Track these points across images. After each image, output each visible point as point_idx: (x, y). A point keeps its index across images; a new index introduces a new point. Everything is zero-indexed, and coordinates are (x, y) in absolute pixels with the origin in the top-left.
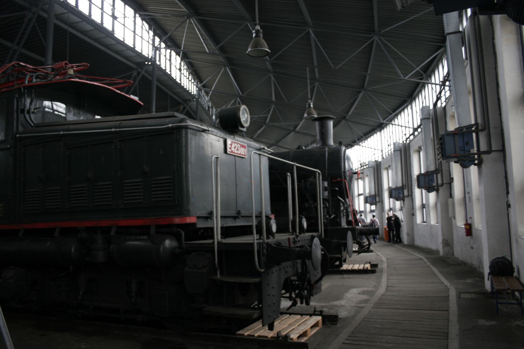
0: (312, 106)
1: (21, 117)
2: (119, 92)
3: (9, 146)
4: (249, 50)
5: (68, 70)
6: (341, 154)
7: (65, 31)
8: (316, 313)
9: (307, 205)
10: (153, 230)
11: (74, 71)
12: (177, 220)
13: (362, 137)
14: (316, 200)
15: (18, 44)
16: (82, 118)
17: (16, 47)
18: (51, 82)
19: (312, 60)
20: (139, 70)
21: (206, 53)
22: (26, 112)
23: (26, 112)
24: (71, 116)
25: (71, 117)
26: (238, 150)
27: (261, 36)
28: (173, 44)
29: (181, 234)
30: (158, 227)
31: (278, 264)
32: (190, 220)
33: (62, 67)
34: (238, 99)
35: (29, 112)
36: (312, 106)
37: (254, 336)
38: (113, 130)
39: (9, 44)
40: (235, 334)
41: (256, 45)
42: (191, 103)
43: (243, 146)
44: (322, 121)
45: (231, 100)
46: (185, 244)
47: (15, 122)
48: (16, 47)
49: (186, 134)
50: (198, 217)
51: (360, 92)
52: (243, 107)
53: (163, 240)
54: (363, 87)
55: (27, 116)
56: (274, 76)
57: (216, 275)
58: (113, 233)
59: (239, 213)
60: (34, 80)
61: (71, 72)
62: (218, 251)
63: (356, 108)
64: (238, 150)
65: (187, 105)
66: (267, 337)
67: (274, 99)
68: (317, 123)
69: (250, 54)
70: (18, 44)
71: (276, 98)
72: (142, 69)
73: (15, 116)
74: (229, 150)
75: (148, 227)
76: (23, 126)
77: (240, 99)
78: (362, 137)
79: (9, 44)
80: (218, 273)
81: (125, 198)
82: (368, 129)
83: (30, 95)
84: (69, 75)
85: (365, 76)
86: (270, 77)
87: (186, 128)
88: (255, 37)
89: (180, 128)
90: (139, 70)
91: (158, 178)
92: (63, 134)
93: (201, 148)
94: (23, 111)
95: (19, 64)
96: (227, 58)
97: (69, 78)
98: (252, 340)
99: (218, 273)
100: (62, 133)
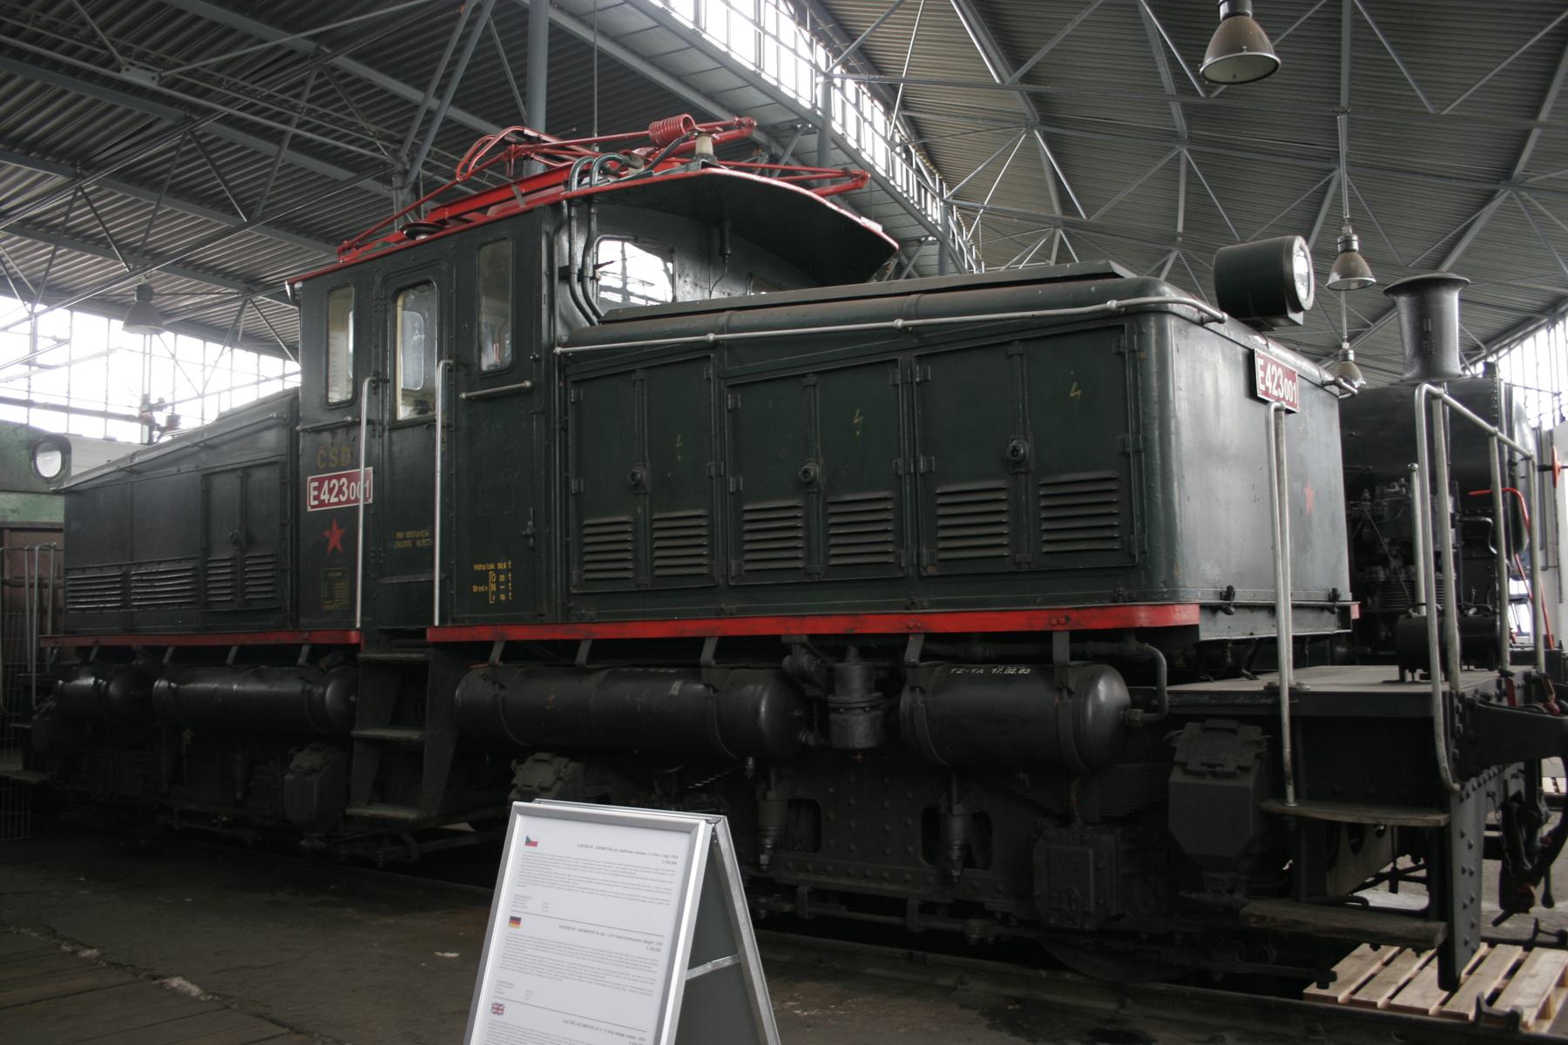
0: (1356, 246)
1: (563, 293)
2: (835, 208)
3: (528, 384)
4: (1208, 61)
5: (698, 142)
6: (1498, 402)
7: (587, 48)
8: (1541, 937)
9: (1382, 575)
10: (1061, 648)
11: (716, 144)
12: (1144, 617)
13: (1478, 348)
14: (1409, 558)
15: (440, 93)
16: (716, 295)
17: (433, 103)
18: (647, 180)
19: (1337, 91)
20: (776, 149)
21: (994, 86)
22: (575, 278)
23: (575, 278)
24: (688, 288)
25: (689, 292)
26: (1278, 386)
27: (1249, 12)
28: (868, 63)
29: (1155, 662)
30: (1077, 636)
31: (1477, 775)
32: (1186, 615)
33: (678, 133)
34: (1060, 232)
35: (581, 278)
36: (1356, 246)
37: (1374, 1005)
38: (899, 323)
39: (414, 95)
40: (1301, 996)
41: (1235, 43)
42: (925, 249)
43: (205, 135)
44: (1423, 291)
45: (1041, 235)
46: (1170, 693)
47: (545, 308)
48: (433, 103)
49: (1162, 332)
50: (1203, 607)
51: (1489, 197)
52: (1299, 242)
53: (1092, 681)
54: (1506, 174)
55: (578, 289)
56: (1190, 151)
57: (1282, 796)
58: (912, 653)
59: (1229, 593)
60: (596, 177)
61: (706, 146)
62: (1292, 718)
63: (1466, 253)
64: (1278, 386)
65: (909, 259)
66: (1425, 1012)
67: (1180, 229)
68: (1403, 302)
69: (1208, 75)
70: (440, 93)
71: (1185, 227)
72: (784, 147)
73: (545, 291)
74: (1260, 387)
75: (1045, 637)
76: (567, 324)
77: (1066, 233)
78: (1478, 348)
79: (414, 95)
80: (1290, 790)
81: (942, 544)
82: (1507, 318)
83: (585, 222)
84: (702, 155)
85: (1527, 134)
86: (1177, 159)
87: (1161, 311)
88: (1226, 16)
89: (1139, 314)
90: (776, 149)
91: (1064, 478)
92: (716, 342)
93: (409, 408)
94: (565, 274)
95: (521, 134)
96: (1038, 100)
97: (705, 165)
98: (1360, 1019)
99: (1290, 790)
100: (711, 337)
